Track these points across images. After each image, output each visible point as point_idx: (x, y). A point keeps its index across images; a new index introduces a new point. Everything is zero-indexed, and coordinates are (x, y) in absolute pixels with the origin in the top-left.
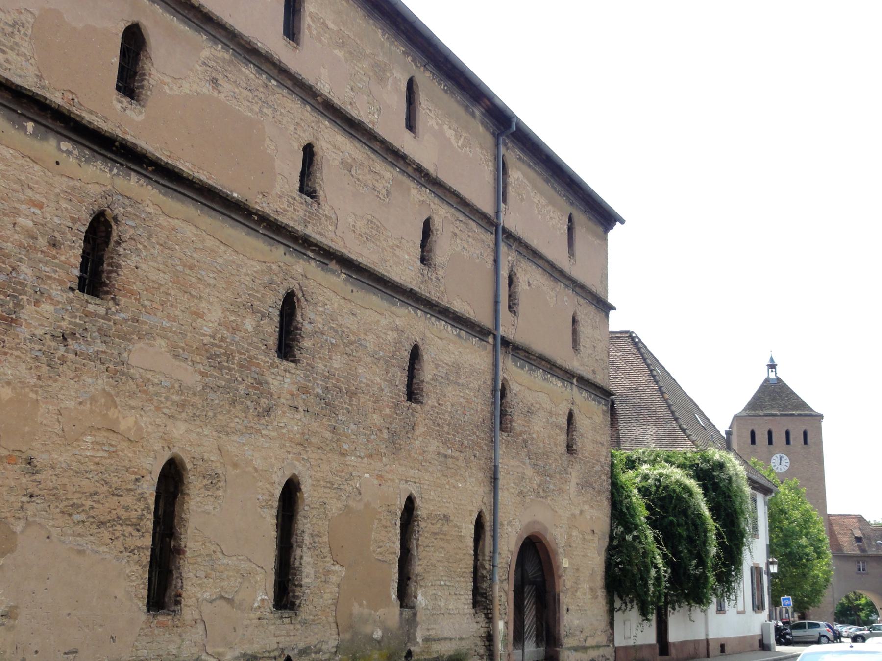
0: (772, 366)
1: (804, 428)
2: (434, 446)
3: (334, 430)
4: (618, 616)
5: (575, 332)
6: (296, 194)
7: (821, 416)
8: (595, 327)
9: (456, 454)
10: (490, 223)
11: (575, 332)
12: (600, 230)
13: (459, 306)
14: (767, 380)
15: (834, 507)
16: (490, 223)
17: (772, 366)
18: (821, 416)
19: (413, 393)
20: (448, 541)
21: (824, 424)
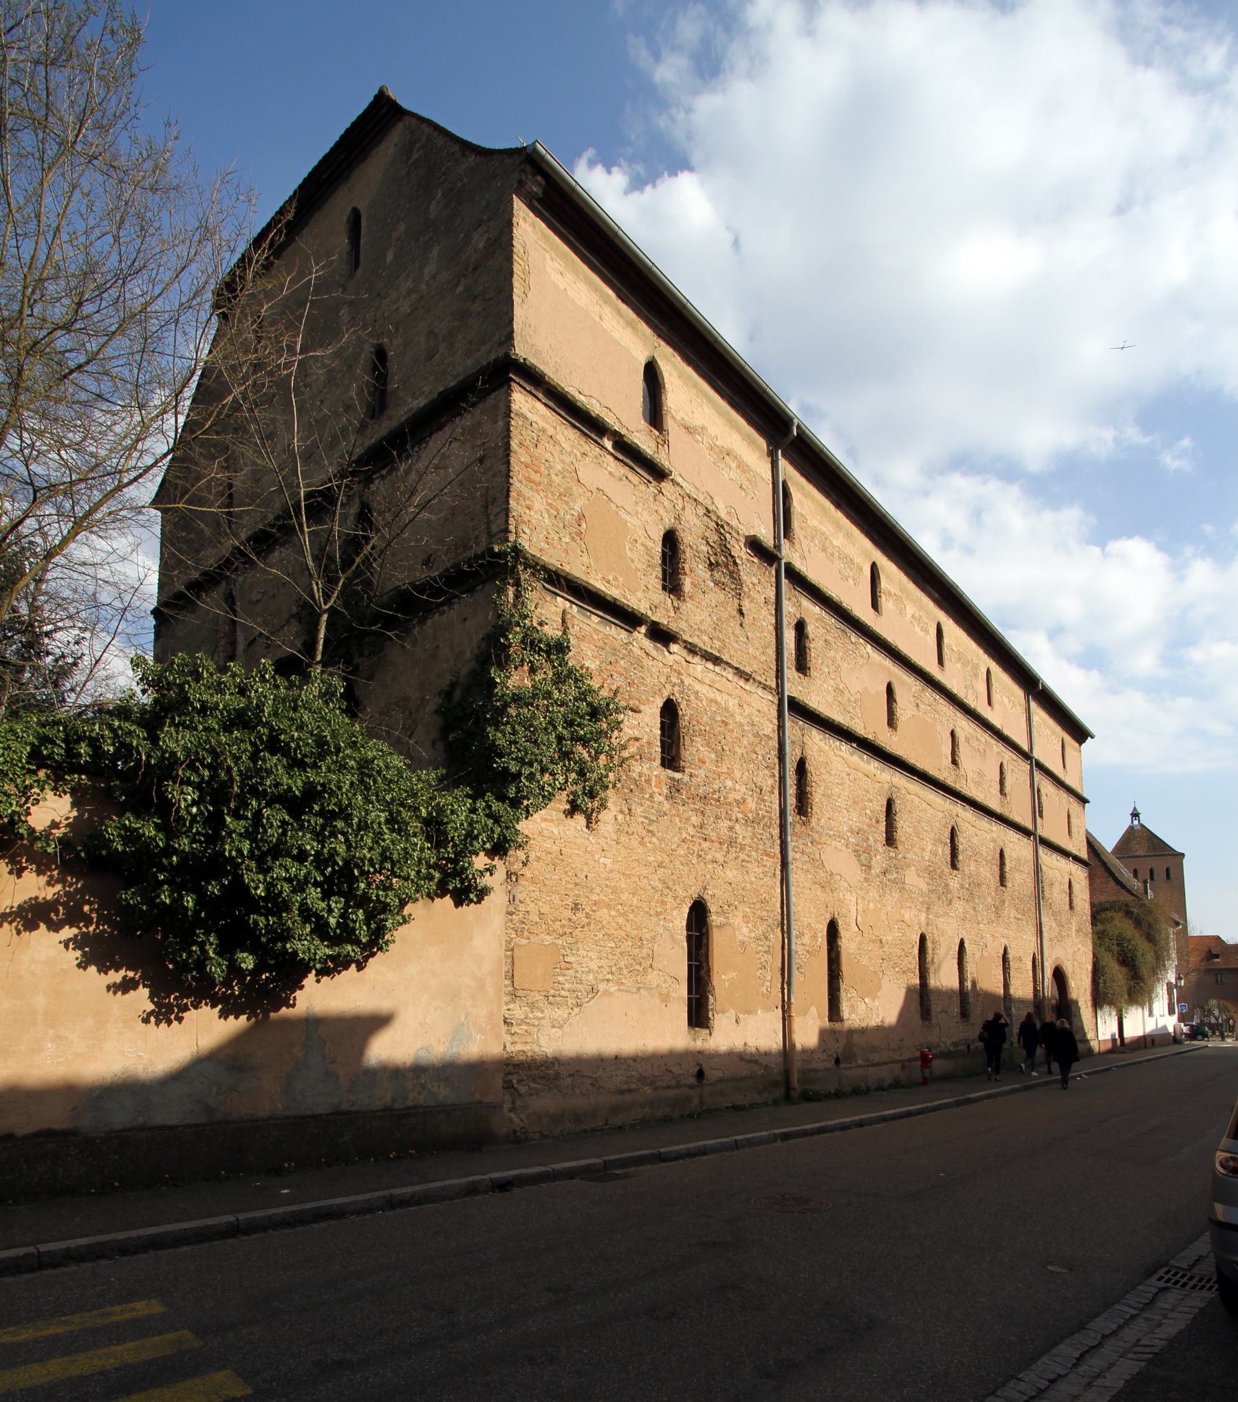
0: (1135, 815)
1: (1167, 866)
2: (1013, 913)
3: (974, 909)
4: (1099, 1012)
5: (1069, 823)
6: (951, 765)
7: (1182, 855)
8: (1078, 818)
9: (1022, 917)
10: (1027, 756)
11: (1069, 823)
12: (1077, 745)
13: (1017, 818)
14: (1131, 828)
15: (798, 1046)
16: (1027, 756)
17: (1135, 815)
18: (1182, 855)
19: (1002, 880)
20: (1022, 973)
21: (1186, 862)
